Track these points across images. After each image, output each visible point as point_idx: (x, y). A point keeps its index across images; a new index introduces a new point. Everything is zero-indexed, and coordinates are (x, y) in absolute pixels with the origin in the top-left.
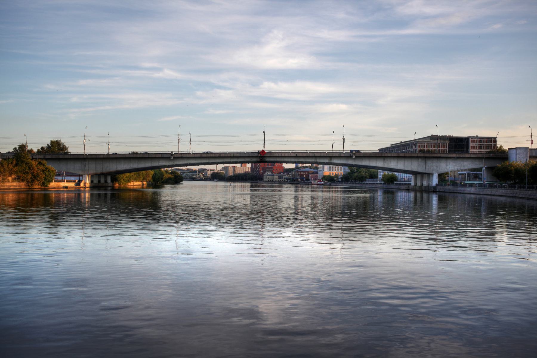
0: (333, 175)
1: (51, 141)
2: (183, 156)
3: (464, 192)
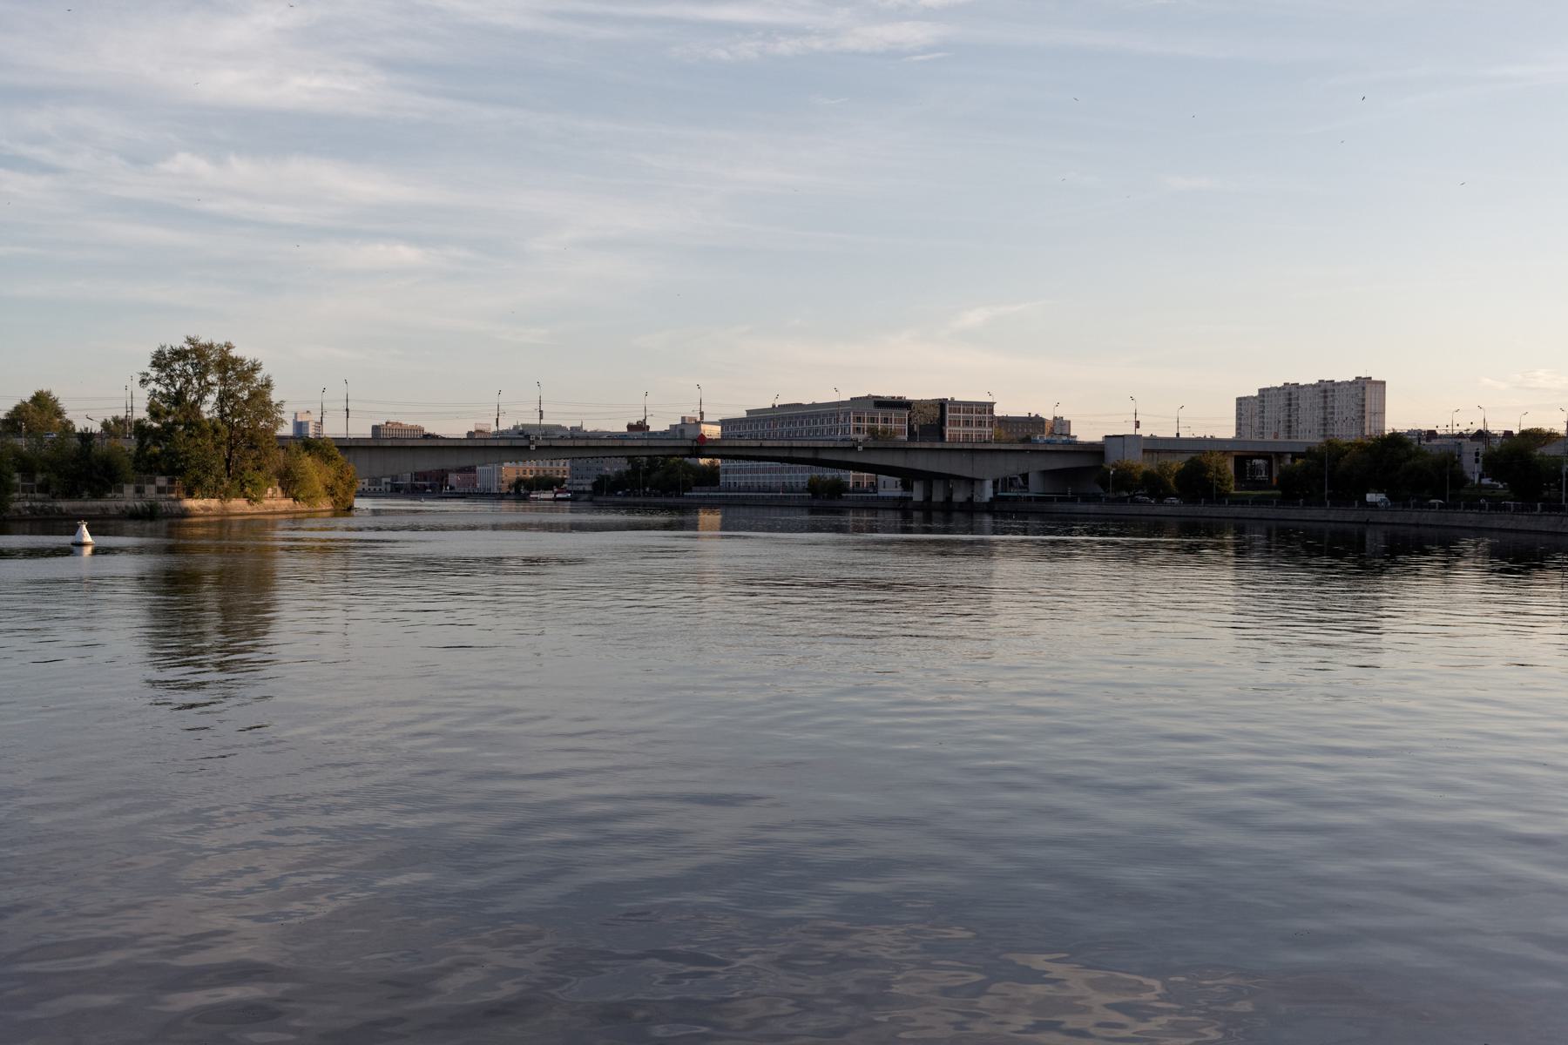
1: (1241, 402)
2: (553, 444)
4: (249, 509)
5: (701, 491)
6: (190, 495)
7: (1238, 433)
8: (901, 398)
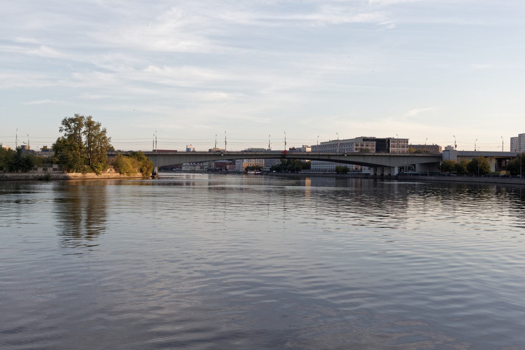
0: (251, 166)
1: (512, 139)
3: (425, 179)
4: (96, 177)
6: (69, 172)
7: (511, 151)
8: (374, 137)
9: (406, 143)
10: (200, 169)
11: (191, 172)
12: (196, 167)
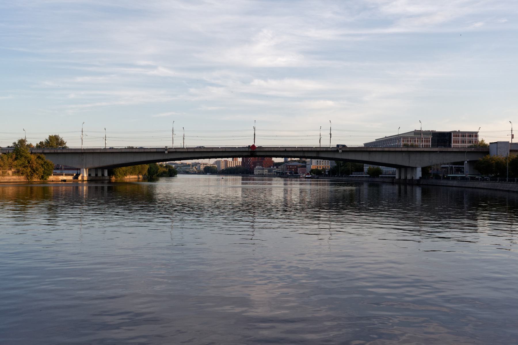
0: (321, 169)
2: (177, 151)
5: (359, 174)
9: (475, 137)
10: (268, 172)
11: (259, 176)
12: (264, 170)
